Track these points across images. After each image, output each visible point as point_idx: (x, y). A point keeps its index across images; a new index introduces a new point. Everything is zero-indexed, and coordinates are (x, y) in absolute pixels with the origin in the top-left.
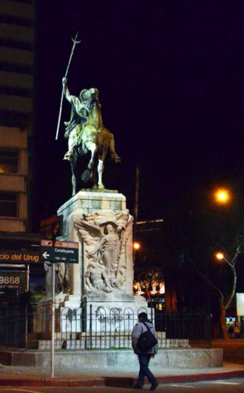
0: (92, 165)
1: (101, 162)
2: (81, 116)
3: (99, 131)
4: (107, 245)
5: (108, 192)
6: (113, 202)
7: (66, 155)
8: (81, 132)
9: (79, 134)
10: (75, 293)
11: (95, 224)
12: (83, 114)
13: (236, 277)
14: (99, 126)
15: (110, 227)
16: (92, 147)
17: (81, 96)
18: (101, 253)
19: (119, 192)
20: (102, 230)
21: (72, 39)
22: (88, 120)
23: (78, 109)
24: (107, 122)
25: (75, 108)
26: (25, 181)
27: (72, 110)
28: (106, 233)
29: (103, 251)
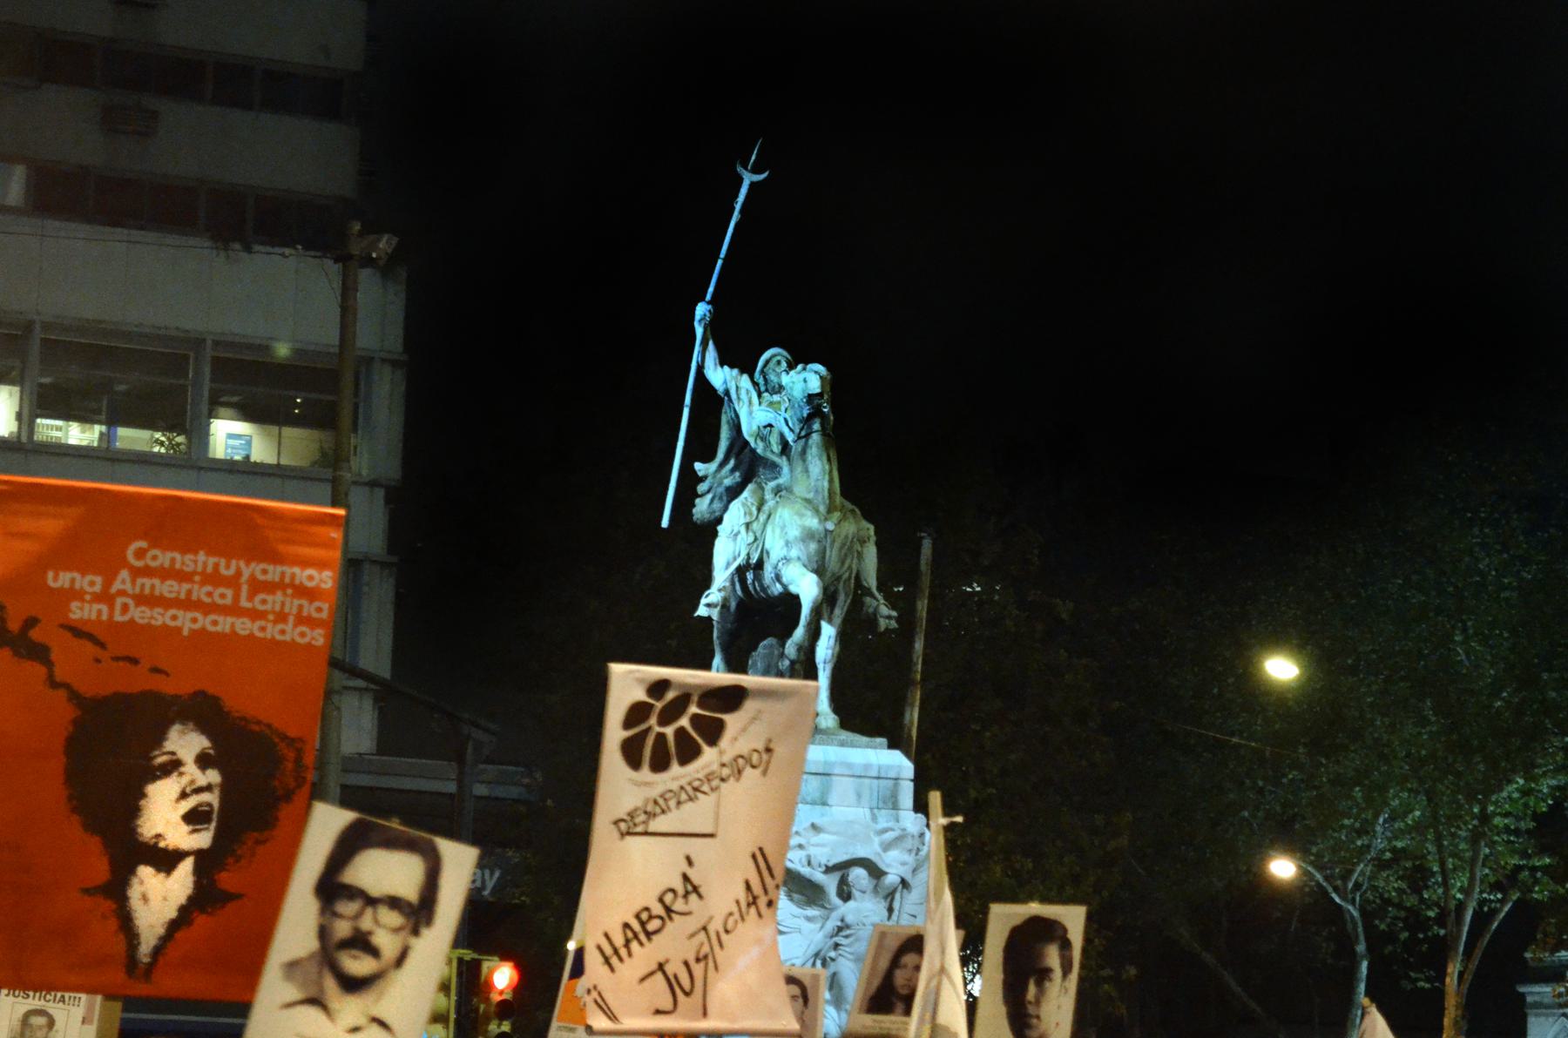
0: (800, 648)
1: (828, 632)
2: (759, 451)
3: (830, 526)
4: (847, 937)
5: (853, 746)
6: (867, 781)
7: (704, 601)
8: (762, 518)
9: (755, 526)
10: (195, 836)
11: (809, 864)
12: (768, 445)
13: (1365, 964)
14: (830, 510)
15: (858, 875)
16: (807, 588)
17: (762, 371)
18: (824, 964)
19: (891, 746)
20: (830, 883)
21: (740, 169)
22: (786, 470)
23: (750, 424)
24: (859, 485)
25: (737, 416)
26: (388, 501)
27: (724, 419)
28: (845, 895)
29: (833, 960)
